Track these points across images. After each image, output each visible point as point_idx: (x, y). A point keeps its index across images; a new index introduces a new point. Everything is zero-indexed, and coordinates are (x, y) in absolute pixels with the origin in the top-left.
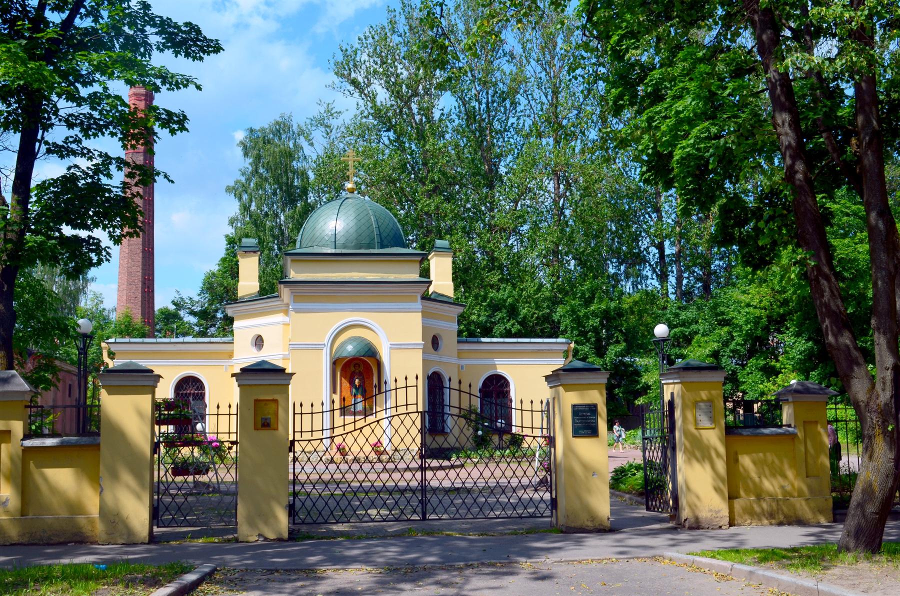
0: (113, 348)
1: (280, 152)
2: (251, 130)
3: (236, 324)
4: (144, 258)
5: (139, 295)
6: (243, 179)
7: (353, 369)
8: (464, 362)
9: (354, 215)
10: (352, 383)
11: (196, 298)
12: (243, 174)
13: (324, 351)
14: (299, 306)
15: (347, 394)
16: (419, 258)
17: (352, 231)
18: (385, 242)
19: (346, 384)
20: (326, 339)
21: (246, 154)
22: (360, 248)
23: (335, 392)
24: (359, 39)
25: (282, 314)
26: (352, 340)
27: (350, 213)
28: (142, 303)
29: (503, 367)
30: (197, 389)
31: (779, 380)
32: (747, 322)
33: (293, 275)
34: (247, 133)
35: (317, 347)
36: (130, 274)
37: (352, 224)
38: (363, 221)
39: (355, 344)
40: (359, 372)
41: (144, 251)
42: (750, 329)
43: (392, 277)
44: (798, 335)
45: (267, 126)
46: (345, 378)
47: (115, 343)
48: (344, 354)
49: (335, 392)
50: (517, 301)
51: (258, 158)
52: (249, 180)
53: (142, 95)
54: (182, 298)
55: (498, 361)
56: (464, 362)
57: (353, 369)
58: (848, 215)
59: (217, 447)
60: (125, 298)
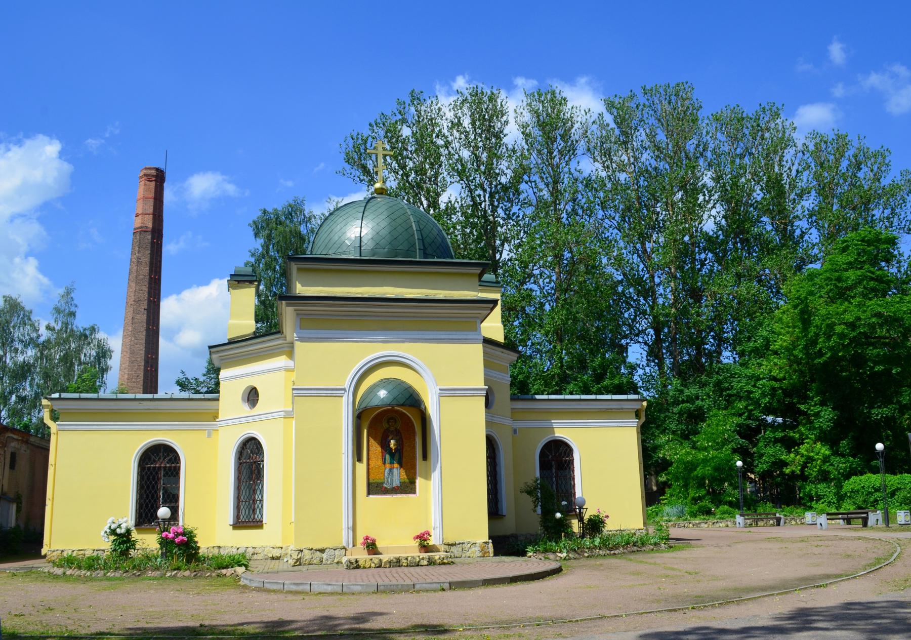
0: (58, 406)
1: (290, 231)
2: (265, 212)
3: (223, 374)
4: (147, 336)
5: (141, 374)
6: (252, 260)
7: (386, 426)
8: (519, 425)
9: (386, 214)
10: (385, 446)
11: (202, 379)
12: (253, 255)
13: (344, 399)
14: (306, 333)
15: (376, 462)
16: (478, 271)
17: (384, 233)
18: (429, 251)
19: (376, 448)
20: (347, 381)
21: (256, 235)
22: (396, 256)
23: (360, 460)
24: (370, 125)
25: (284, 357)
26: (385, 383)
27: (380, 211)
28: (144, 382)
29: (563, 431)
30: (170, 461)
31: (803, 449)
32: (764, 395)
33: (300, 289)
34: (260, 214)
35: (334, 393)
36: (132, 352)
37: (384, 224)
38: (399, 221)
39: (390, 387)
40: (395, 432)
41: (147, 330)
42: (769, 402)
43: (441, 294)
44: (822, 403)
45: (280, 208)
46: (375, 440)
47: (60, 399)
48: (375, 402)
49: (360, 460)
50: (528, 377)
51: (269, 238)
52: (258, 261)
53: (153, 176)
54: (187, 379)
55: (556, 423)
56: (519, 425)
57: (386, 426)
58: (872, 279)
59: (182, 543)
60: (126, 377)
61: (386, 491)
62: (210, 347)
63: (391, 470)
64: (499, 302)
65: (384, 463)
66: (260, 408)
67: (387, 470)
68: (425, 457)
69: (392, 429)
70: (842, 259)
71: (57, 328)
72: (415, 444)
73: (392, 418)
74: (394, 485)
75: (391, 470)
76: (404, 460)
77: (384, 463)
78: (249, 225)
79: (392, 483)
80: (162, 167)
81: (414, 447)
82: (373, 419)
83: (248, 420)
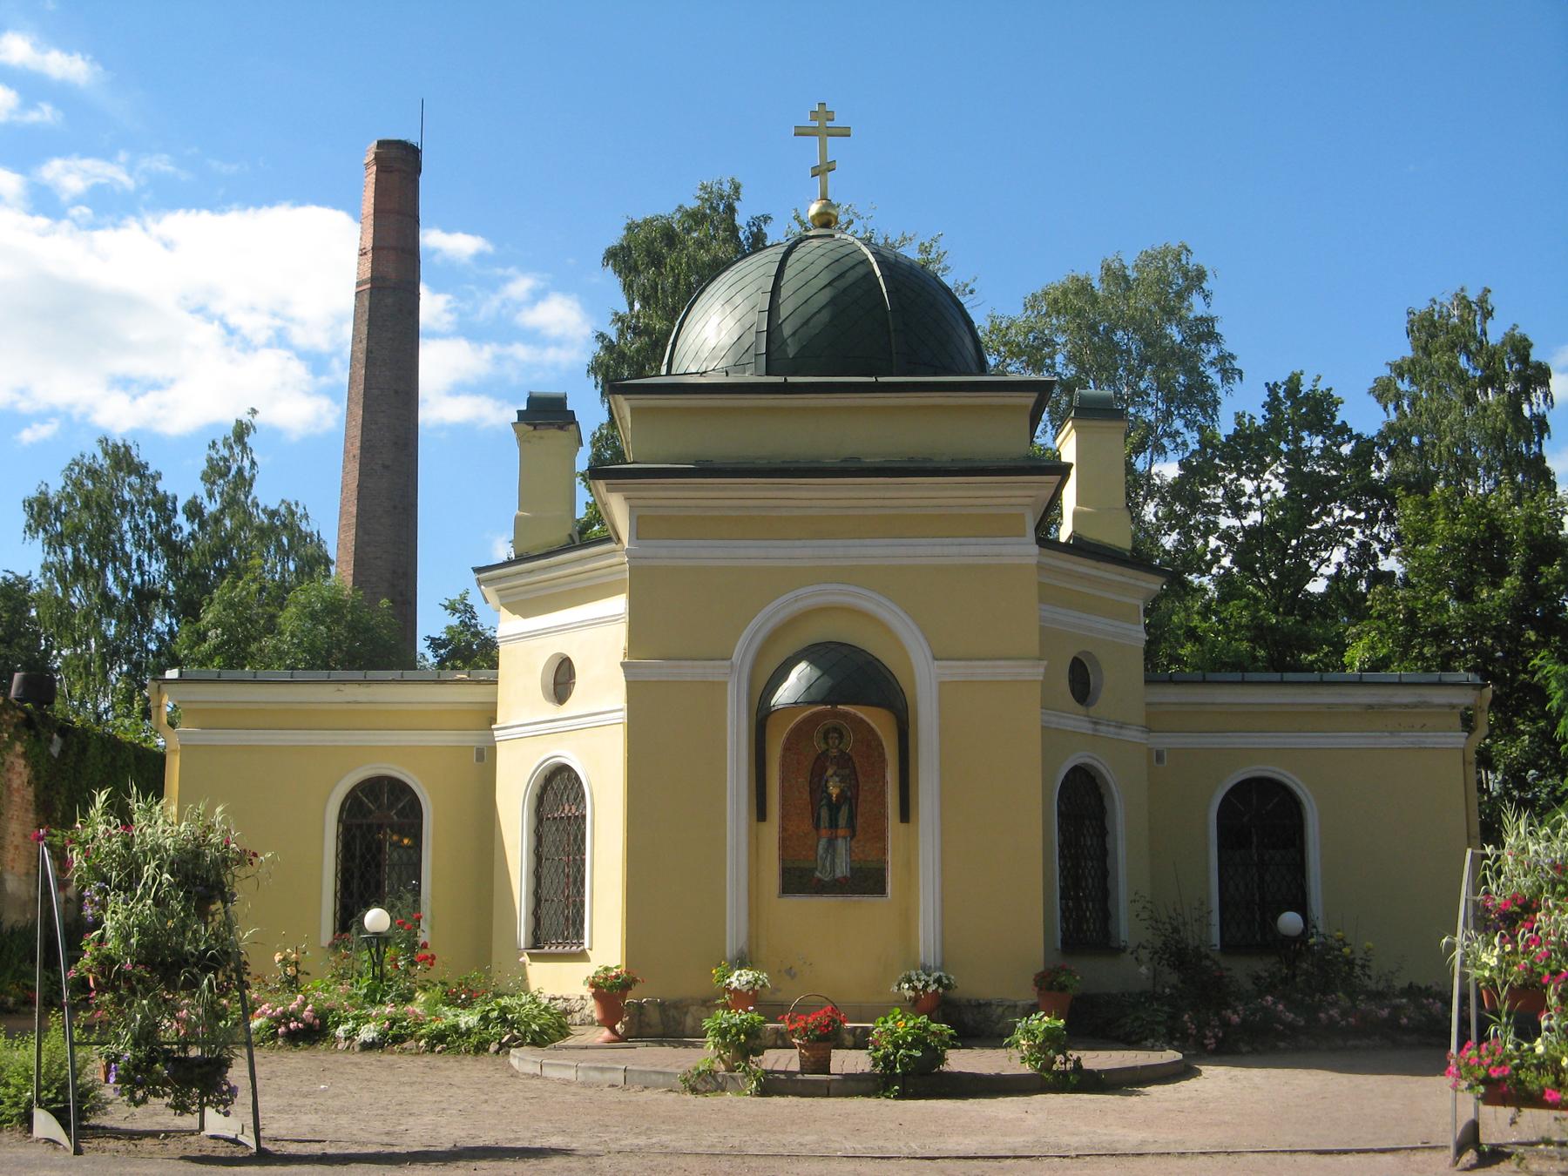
57: (820, 746)
61: (821, 888)
62: (477, 570)
63: (831, 843)
64: (1073, 472)
65: (817, 827)
66: (573, 705)
67: (823, 842)
68: (905, 815)
69: (834, 752)
70: (196, 559)
71: (211, 507)
72: (884, 783)
73: (835, 729)
74: (839, 874)
75: (831, 843)
76: (860, 820)
77: (817, 827)
78: (1515, 326)
79: (833, 870)
80: (413, 139)
81: (882, 795)
82: (793, 730)
83: (551, 729)
